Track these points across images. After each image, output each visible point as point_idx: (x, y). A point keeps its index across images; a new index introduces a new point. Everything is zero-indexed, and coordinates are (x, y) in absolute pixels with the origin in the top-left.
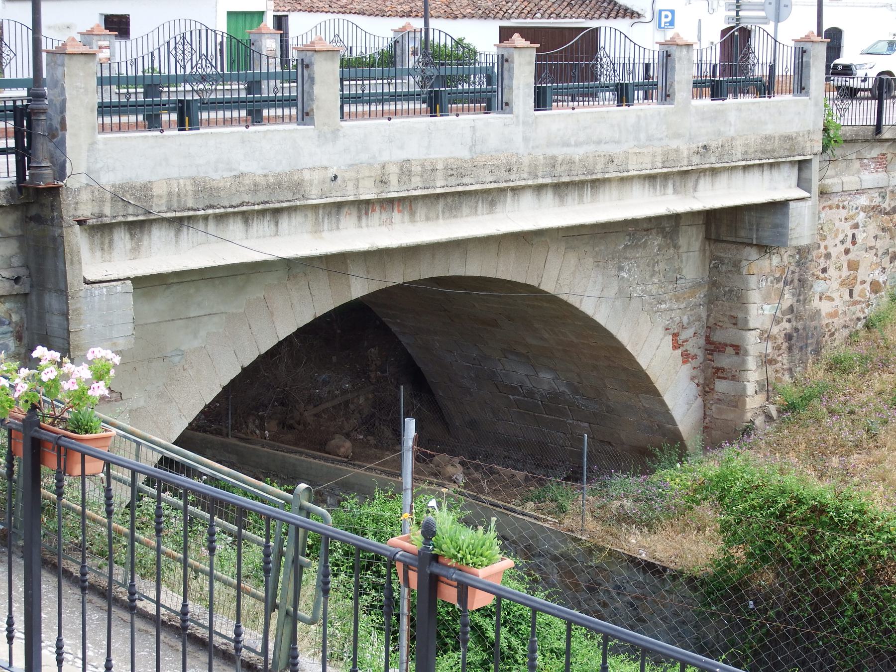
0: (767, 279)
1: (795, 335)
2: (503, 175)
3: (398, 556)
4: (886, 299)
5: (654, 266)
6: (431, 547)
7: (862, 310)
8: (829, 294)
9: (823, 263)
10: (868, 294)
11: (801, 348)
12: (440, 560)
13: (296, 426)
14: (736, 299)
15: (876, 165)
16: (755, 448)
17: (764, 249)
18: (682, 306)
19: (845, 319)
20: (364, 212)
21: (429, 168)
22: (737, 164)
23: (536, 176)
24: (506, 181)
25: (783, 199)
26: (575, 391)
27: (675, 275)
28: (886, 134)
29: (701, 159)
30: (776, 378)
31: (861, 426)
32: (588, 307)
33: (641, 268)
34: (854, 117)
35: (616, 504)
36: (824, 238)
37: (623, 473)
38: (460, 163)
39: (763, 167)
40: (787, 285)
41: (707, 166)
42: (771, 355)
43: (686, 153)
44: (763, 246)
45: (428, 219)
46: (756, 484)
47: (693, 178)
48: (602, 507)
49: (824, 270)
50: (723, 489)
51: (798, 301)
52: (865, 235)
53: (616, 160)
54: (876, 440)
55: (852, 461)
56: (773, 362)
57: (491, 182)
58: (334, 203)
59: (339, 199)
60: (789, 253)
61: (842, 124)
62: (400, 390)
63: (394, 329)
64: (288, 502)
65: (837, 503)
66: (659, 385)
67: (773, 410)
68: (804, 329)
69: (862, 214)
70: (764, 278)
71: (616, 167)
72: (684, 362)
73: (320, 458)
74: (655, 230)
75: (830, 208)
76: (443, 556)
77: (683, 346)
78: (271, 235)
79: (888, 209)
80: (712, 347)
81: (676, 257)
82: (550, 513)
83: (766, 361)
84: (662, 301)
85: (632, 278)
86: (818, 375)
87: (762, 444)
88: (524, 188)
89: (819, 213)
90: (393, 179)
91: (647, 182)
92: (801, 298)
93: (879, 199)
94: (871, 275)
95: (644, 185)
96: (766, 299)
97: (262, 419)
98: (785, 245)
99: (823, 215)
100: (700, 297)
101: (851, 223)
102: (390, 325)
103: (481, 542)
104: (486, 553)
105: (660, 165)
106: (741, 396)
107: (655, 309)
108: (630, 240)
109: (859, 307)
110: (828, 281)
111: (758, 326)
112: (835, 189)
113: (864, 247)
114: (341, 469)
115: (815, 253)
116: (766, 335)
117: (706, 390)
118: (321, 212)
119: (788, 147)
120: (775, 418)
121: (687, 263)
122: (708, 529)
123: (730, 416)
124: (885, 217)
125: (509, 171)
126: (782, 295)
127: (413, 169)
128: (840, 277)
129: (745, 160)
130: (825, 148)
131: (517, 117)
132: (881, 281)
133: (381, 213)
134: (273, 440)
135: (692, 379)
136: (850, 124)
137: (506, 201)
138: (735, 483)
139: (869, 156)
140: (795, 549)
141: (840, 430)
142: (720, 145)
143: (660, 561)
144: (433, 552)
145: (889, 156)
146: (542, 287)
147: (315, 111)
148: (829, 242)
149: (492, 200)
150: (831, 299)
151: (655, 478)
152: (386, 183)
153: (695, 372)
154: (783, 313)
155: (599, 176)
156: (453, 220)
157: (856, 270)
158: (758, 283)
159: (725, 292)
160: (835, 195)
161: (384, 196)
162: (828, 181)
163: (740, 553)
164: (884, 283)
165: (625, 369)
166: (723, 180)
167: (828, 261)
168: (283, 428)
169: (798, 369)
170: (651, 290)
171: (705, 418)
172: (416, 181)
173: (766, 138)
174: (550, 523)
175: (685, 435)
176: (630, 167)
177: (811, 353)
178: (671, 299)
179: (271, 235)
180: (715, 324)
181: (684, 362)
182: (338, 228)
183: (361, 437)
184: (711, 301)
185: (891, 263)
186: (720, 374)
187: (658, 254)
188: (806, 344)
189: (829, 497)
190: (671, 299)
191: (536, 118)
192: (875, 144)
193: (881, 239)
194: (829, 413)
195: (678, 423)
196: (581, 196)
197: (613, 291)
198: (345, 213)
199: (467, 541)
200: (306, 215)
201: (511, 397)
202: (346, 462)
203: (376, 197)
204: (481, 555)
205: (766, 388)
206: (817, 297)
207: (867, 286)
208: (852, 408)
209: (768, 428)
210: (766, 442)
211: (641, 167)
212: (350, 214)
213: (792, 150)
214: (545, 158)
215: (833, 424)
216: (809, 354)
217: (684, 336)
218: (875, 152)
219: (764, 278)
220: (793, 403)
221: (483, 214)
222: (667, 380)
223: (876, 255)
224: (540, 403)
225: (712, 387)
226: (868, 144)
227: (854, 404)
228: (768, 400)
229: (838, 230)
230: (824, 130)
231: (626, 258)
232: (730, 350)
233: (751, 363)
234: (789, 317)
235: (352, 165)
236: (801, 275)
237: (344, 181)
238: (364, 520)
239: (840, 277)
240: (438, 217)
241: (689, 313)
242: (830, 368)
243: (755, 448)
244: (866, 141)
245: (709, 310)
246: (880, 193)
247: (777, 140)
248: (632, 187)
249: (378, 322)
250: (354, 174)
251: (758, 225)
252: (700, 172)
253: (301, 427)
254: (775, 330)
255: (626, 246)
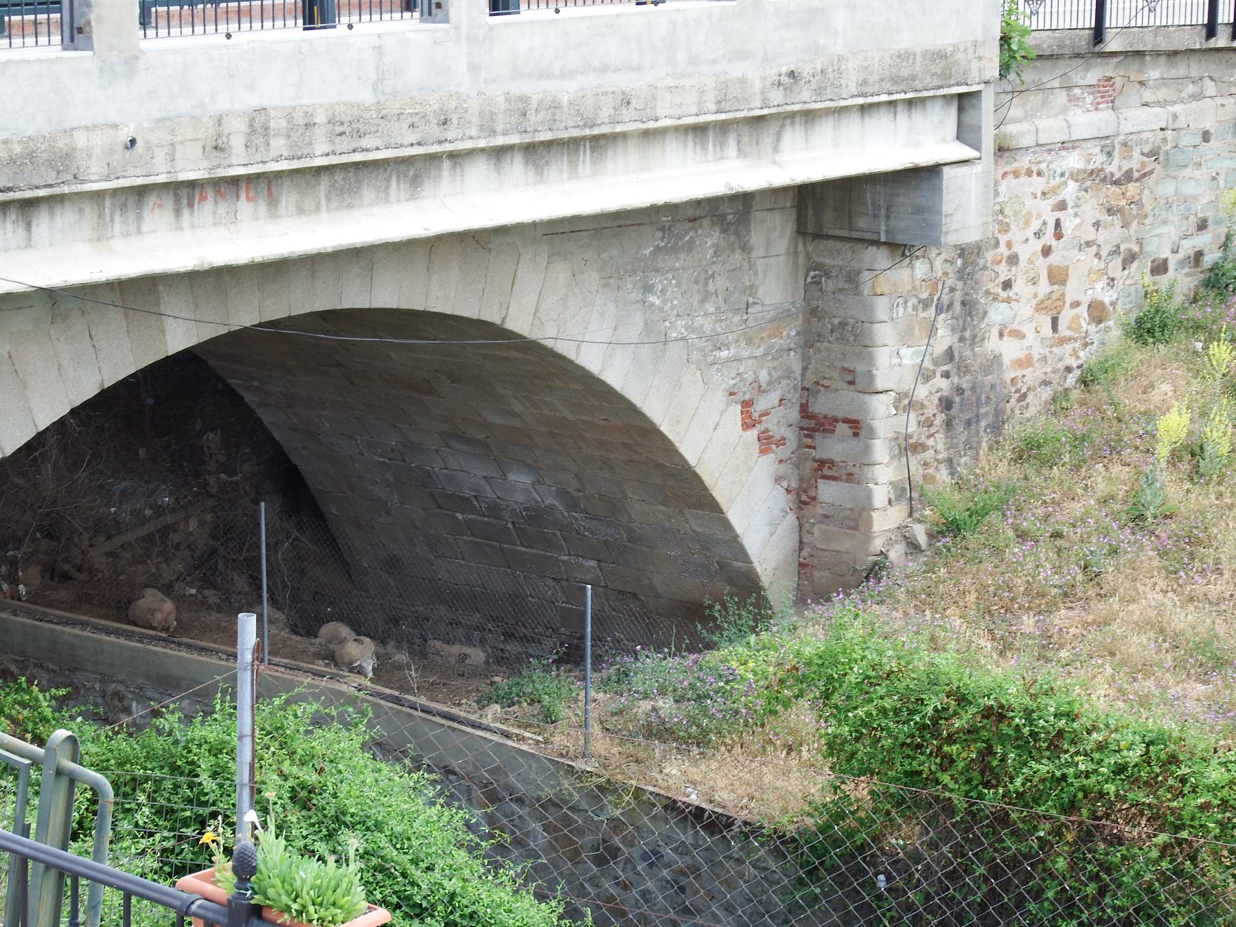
0: (906, 302)
1: (957, 399)
2: (436, 131)
3: (193, 908)
4: (1116, 333)
5: (706, 283)
6: (249, 893)
7: (1075, 354)
8: (1015, 326)
9: (1004, 272)
10: (1084, 325)
11: (968, 423)
12: (265, 914)
13: (75, 574)
14: (852, 339)
15: (1095, 98)
16: (888, 601)
17: (900, 249)
18: (759, 352)
19: (1045, 370)
20: (185, 202)
21: (302, 122)
22: (850, 102)
23: (493, 133)
24: (440, 142)
25: (932, 163)
26: (573, 505)
27: (744, 298)
28: (1113, 44)
29: (786, 95)
30: (925, 477)
31: (1073, 559)
32: (590, 359)
33: (684, 288)
34: (1055, 9)
35: (646, 705)
36: (1005, 228)
37: (658, 649)
38: (356, 112)
39: (895, 107)
40: (941, 312)
41: (796, 108)
42: (915, 437)
43: (758, 85)
44: (898, 246)
45: (300, 211)
46: (888, 668)
47: (773, 127)
48: (620, 713)
49: (1007, 285)
50: (830, 679)
51: (962, 339)
52: (1077, 221)
53: (634, 102)
54: (1098, 584)
55: (1057, 621)
56: (920, 449)
57: (412, 145)
58: (132, 188)
59: (140, 181)
60: (944, 256)
61: (1034, 27)
62: (258, 512)
63: (249, 398)
64: (36, 763)
65: (1027, 701)
66: (720, 493)
67: (920, 533)
68: (973, 389)
69: (1072, 185)
70: (901, 300)
71: (634, 112)
72: (764, 451)
73: (118, 633)
74: (708, 219)
75: (1016, 174)
76: (270, 907)
77: (760, 422)
78: (18, 247)
79: (1117, 175)
80: (812, 424)
81: (746, 266)
82: (527, 726)
83: (907, 447)
84: (723, 344)
85: (669, 305)
86: (1002, 470)
87: (901, 594)
88: (471, 153)
89: (996, 184)
90: (237, 143)
91: (690, 138)
92: (968, 334)
93: (1101, 158)
94: (1090, 292)
95: (685, 142)
96: (906, 337)
97: (13, 563)
98: (937, 243)
99: (1003, 188)
100: (788, 336)
101: (1053, 200)
102: (241, 392)
103: (333, 883)
104: (343, 901)
105: (713, 108)
106: (864, 509)
107: (710, 359)
108: (664, 237)
109: (1068, 348)
110: (1013, 304)
111: (891, 385)
112: (1024, 143)
113: (1075, 242)
114: (155, 653)
115: (989, 255)
116: (906, 402)
117: (803, 499)
118: (108, 203)
119: (939, 71)
120: (924, 547)
121: (765, 276)
122: (805, 748)
123: (846, 545)
124: (1114, 188)
125: (445, 123)
126: (932, 331)
127: (272, 124)
128: (1036, 296)
129: (864, 95)
130: (1005, 68)
131: (457, 28)
132: (1107, 301)
133: (216, 203)
134: (33, 603)
135: (778, 480)
136: (1048, 27)
137: (440, 176)
138: (851, 668)
139: (1082, 82)
140: (956, 782)
141: (1037, 567)
142: (819, 70)
143: (724, 807)
144: (252, 902)
145: (1118, 82)
146: (509, 325)
147: (93, 24)
148: (1015, 235)
149: (416, 177)
150: (1018, 335)
151: (712, 657)
152: (223, 150)
153: (782, 469)
154: (936, 362)
155: (606, 129)
156: (346, 213)
157: (1063, 282)
158: (891, 309)
159: (833, 325)
160: (1024, 151)
161: (221, 173)
162: (1011, 129)
163: (863, 792)
164: (1113, 304)
165: (658, 466)
166: (825, 130)
167: (1014, 269)
168: (52, 578)
169: (963, 460)
170: (702, 326)
171: (801, 549)
172: (279, 145)
173: (899, 56)
174: (528, 742)
175: (765, 581)
176: (659, 113)
177: (985, 431)
178: (737, 341)
179: (18, 247)
180: (817, 383)
181: (764, 451)
182: (139, 232)
183: (193, 591)
184: (809, 342)
185: (1124, 269)
186: (826, 472)
187: (714, 263)
188: (977, 416)
189: (1013, 690)
190: (737, 341)
191: (491, 28)
192: (1093, 61)
193: (1105, 227)
194: (1018, 536)
195: (754, 558)
196: (573, 165)
197: (634, 329)
198: (152, 204)
199: (309, 881)
200: (81, 210)
201: (459, 516)
202: (164, 640)
203: (207, 176)
204: (334, 904)
205: (908, 493)
206: (995, 332)
207: (1083, 311)
208: (1057, 527)
209: (912, 566)
210: (908, 592)
211: (678, 112)
212: (160, 206)
213: (945, 77)
214: (508, 100)
215: (1024, 556)
216: (982, 433)
217: (761, 405)
218: (1094, 75)
219: (901, 300)
220: (954, 521)
221: (399, 201)
222: (733, 483)
223: (1097, 255)
224: (510, 525)
225: (812, 493)
226: (1080, 61)
227: (1061, 521)
228: (910, 515)
229: (1029, 213)
230: (1002, 38)
231: (657, 270)
232: (842, 428)
233: (881, 450)
234: (945, 368)
235: (162, 120)
236: (967, 294)
237: (149, 149)
238: (195, 749)
239: (1036, 296)
240: (318, 208)
241: (770, 365)
242: (1019, 457)
243: (888, 601)
244: (1078, 56)
245: (806, 359)
246: (1103, 147)
247: (919, 59)
248: (664, 142)
249: (220, 386)
250: (166, 136)
251: (888, 208)
252: (785, 118)
253: (83, 577)
254: (922, 392)
255: (658, 249)
